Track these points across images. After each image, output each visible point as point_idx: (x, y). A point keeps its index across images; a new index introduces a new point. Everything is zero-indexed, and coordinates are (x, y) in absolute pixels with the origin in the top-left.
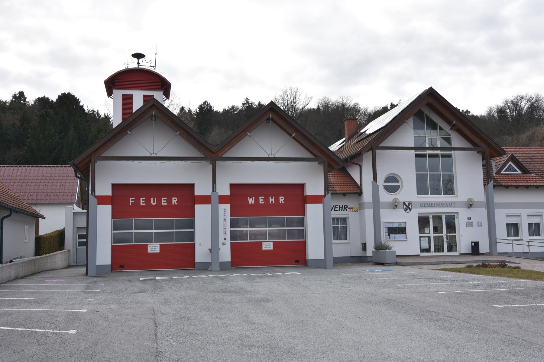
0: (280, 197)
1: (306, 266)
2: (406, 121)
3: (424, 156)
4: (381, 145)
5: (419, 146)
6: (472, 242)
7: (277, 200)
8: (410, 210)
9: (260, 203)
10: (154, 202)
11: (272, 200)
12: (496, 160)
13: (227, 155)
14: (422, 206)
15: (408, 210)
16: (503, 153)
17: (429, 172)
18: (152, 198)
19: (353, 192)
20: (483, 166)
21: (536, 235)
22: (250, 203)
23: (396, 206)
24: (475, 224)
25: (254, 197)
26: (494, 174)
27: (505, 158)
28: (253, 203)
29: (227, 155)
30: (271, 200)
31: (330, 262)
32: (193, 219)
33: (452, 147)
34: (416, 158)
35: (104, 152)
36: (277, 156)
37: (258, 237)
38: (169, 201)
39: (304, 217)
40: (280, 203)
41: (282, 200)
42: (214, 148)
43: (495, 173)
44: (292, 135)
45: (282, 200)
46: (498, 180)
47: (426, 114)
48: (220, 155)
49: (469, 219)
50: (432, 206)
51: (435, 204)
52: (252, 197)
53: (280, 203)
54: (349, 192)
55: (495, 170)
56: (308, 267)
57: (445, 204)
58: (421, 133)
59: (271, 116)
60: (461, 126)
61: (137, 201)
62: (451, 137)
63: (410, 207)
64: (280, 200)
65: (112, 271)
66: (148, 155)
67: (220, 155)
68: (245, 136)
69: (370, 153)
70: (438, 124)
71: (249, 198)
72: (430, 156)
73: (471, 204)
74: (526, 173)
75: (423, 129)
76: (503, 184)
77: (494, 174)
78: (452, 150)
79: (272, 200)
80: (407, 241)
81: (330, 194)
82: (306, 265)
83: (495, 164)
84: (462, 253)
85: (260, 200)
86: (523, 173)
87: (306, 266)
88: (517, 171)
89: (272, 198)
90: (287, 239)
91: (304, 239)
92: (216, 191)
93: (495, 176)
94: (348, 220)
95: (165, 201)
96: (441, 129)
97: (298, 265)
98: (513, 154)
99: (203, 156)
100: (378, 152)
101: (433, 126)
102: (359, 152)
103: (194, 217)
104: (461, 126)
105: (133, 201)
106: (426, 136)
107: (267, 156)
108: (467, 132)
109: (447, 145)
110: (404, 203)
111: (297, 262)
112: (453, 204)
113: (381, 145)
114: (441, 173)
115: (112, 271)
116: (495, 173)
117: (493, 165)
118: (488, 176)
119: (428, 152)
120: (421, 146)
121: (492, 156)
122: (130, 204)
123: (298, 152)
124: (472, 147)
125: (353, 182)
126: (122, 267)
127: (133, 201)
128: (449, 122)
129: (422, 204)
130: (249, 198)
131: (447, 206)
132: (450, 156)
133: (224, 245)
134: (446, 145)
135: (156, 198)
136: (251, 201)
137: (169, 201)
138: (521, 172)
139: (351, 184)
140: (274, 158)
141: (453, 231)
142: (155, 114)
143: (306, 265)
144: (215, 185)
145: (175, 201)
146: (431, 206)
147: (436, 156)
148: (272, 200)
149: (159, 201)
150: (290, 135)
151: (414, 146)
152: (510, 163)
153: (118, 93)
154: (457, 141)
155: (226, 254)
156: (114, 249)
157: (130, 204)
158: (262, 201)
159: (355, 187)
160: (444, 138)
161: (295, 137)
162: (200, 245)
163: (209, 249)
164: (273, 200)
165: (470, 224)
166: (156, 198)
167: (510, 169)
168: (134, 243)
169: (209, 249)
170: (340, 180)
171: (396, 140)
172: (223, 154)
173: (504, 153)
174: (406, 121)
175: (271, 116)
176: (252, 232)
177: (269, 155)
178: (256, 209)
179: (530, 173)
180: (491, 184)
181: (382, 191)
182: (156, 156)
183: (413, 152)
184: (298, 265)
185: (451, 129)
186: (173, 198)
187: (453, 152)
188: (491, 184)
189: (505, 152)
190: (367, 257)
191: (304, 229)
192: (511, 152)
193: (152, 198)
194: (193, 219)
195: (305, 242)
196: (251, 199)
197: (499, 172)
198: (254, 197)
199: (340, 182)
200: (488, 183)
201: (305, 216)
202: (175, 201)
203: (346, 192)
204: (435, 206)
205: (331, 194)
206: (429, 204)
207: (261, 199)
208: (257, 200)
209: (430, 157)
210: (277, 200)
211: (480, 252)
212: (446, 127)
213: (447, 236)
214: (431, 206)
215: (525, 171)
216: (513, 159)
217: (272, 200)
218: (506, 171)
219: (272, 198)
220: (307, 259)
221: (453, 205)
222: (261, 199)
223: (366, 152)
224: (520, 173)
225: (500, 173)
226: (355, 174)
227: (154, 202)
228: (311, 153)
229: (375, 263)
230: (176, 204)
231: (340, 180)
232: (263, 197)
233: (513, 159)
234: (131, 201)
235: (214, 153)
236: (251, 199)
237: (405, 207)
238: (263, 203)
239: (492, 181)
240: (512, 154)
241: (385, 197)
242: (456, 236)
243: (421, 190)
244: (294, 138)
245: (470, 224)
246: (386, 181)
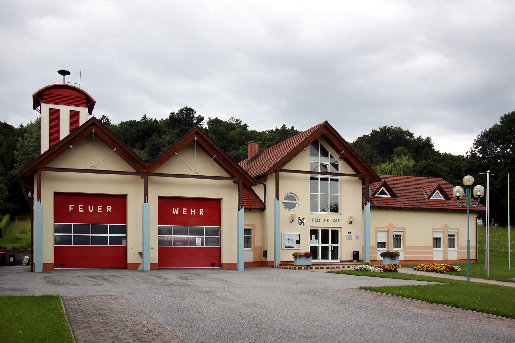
0: (108, 207)
1: (221, 268)
2: (304, 148)
3: (317, 179)
4: (283, 168)
5: (313, 171)
6: (354, 252)
7: (197, 212)
8: (304, 224)
9: (80, 211)
10: (91, 210)
11: (193, 212)
12: (372, 185)
13: (157, 171)
14: (313, 221)
15: (302, 224)
16: (379, 180)
17: (320, 193)
18: (89, 206)
19: (258, 207)
20: (363, 189)
21: (335, 246)
22: (174, 213)
23: (352, 222)
24: (354, 237)
25: (178, 209)
26: (370, 197)
27: (379, 184)
28: (177, 213)
29: (157, 171)
30: (192, 212)
31: (241, 266)
32: (125, 225)
33: (340, 173)
34: (311, 180)
35: (156, 169)
36: (98, 169)
37: (177, 243)
38: (104, 209)
39: (220, 227)
40: (108, 211)
41: (110, 209)
42: (147, 164)
43: (427, 199)
44: (213, 156)
45: (201, 212)
46: (374, 201)
47: (320, 143)
48: (151, 171)
49: (349, 233)
50: (322, 221)
51: (324, 220)
52: (176, 208)
53: (108, 211)
54: (254, 207)
55: (370, 194)
56: (222, 268)
57: (332, 220)
58: (315, 159)
59: (196, 139)
60: (348, 156)
61: (76, 208)
62: (339, 164)
63: (304, 221)
64: (108, 209)
65: (54, 268)
66: (191, 173)
67: (151, 171)
68: (173, 155)
69: (275, 173)
70: (330, 153)
71: (173, 209)
72: (322, 179)
73: (352, 221)
74: (394, 197)
75: (317, 156)
76: (377, 205)
77: (370, 197)
78: (339, 176)
79: (99, 209)
80: (300, 249)
81: (244, 208)
82: (126, 268)
83: (371, 188)
84: (343, 260)
85: (99, 209)
86: (392, 197)
87: (126, 269)
88: (387, 195)
89: (193, 210)
90: (189, 245)
91: (219, 246)
92: (147, 202)
93: (371, 199)
94: (252, 231)
95: (82, 208)
96: (331, 157)
97: (214, 267)
98: (386, 181)
99: (135, 171)
100: (280, 173)
101: (326, 154)
102: (265, 173)
103: (125, 222)
104: (348, 156)
105: (72, 208)
106: (319, 162)
107: (191, 174)
108: (353, 161)
109: (336, 171)
110: (299, 218)
111: (213, 265)
112: (338, 220)
113: (283, 168)
114: (330, 194)
115: (54, 268)
116: (371, 196)
117: (370, 189)
118: (366, 199)
119: (320, 176)
120: (314, 171)
121: (370, 182)
122: (70, 210)
123: (218, 171)
124: (355, 173)
125: (257, 199)
126: (63, 265)
127: (72, 208)
128: (339, 152)
129: (313, 219)
130: (173, 209)
131: (333, 221)
132: (337, 180)
133: (152, 249)
134: (335, 171)
135: (92, 206)
136: (176, 212)
137: (104, 209)
138: (444, 198)
139: (256, 201)
140: (197, 175)
141: (57, 238)
142: (94, 132)
143: (126, 268)
144: (146, 197)
145: (109, 209)
146: (320, 221)
147: (327, 179)
148: (193, 212)
149: (96, 209)
150: (211, 156)
151: (309, 171)
152: (383, 188)
153: (46, 108)
154: (344, 168)
155: (153, 256)
156: (56, 249)
157: (70, 210)
158: (100, 210)
159: (259, 203)
160: (333, 165)
161: (216, 158)
162: (132, 248)
163: (138, 252)
164: (194, 212)
165: (349, 237)
166: (92, 206)
167: (383, 193)
168: (73, 244)
169: (138, 252)
170: (246, 196)
171: (295, 164)
172: (153, 171)
173: (380, 180)
174: (304, 148)
175: (196, 139)
176: (175, 239)
177: (193, 173)
178: (180, 219)
179: (397, 197)
180: (369, 204)
181: (282, 208)
182: (95, 169)
183: (308, 176)
184: (214, 267)
185: (340, 158)
186: (108, 206)
187: (339, 177)
188: (369, 204)
189: (381, 179)
190: (267, 262)
191: (219, 238)
192: (384, 179)
193: (89, 206)
194: (125, 225)
195: (220, 248)
196: (176, 210)
197: (373, 195)
198: (178, 209)
199: (246, 198)
200: (366, 204)
201: (220, 226)
202: (109, 209)
203: (251, 207)
204: (324, 221)
205: (245, 208)
206: (319, 220)
207: (100, 208)
208: (180, 212)
209: (332, 181)
210: (197, 212)
211: (360, 260)
212: (336, 156)
213: (332, 246)
214: (320, 221)
215: (393, 195)
216: (385, 185)
217: (193, 212)
218: (379, 194)
219: (193, 210)
220: (127, 262)
221: (338, 221)
222: (100, 208)
223: (271, 173)
224: (390, 196)
225: (374, 196)
226: (258, 191)
227: (91, 210)
228: (228, 172)
229: (312, 268)
230: (110, 212)
231: (246, 196)
232: (101, 206)
233: (385, 185)
234: (70, 208)
235: (146, 169)
236: (176, 210)
237: (300, 221)
238: (186, 214)
239: (369, 202)
240: (384, 181)
241: (286, 213)
242: (338, 246)
243: (313, 208)
244: (214, 159)
245: (349, 237)
246: (285, 199)
